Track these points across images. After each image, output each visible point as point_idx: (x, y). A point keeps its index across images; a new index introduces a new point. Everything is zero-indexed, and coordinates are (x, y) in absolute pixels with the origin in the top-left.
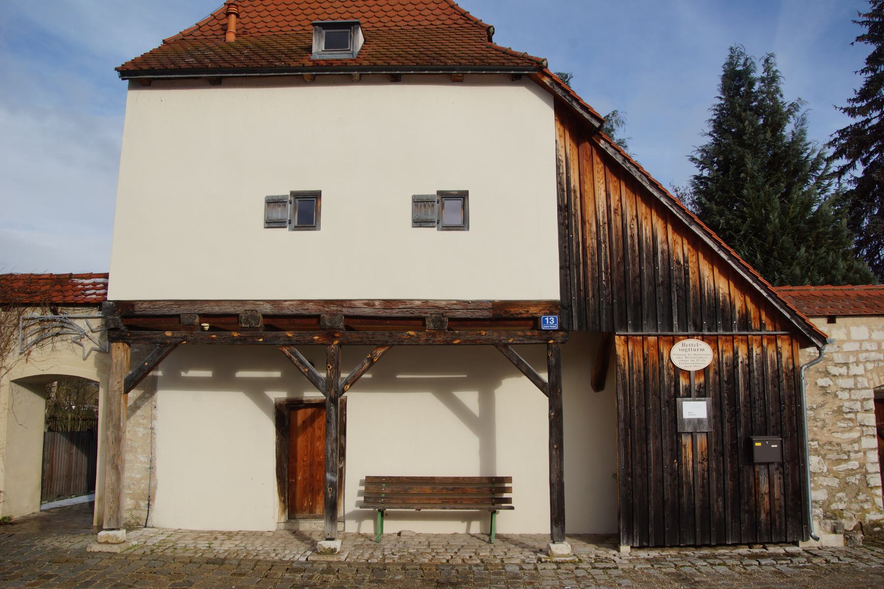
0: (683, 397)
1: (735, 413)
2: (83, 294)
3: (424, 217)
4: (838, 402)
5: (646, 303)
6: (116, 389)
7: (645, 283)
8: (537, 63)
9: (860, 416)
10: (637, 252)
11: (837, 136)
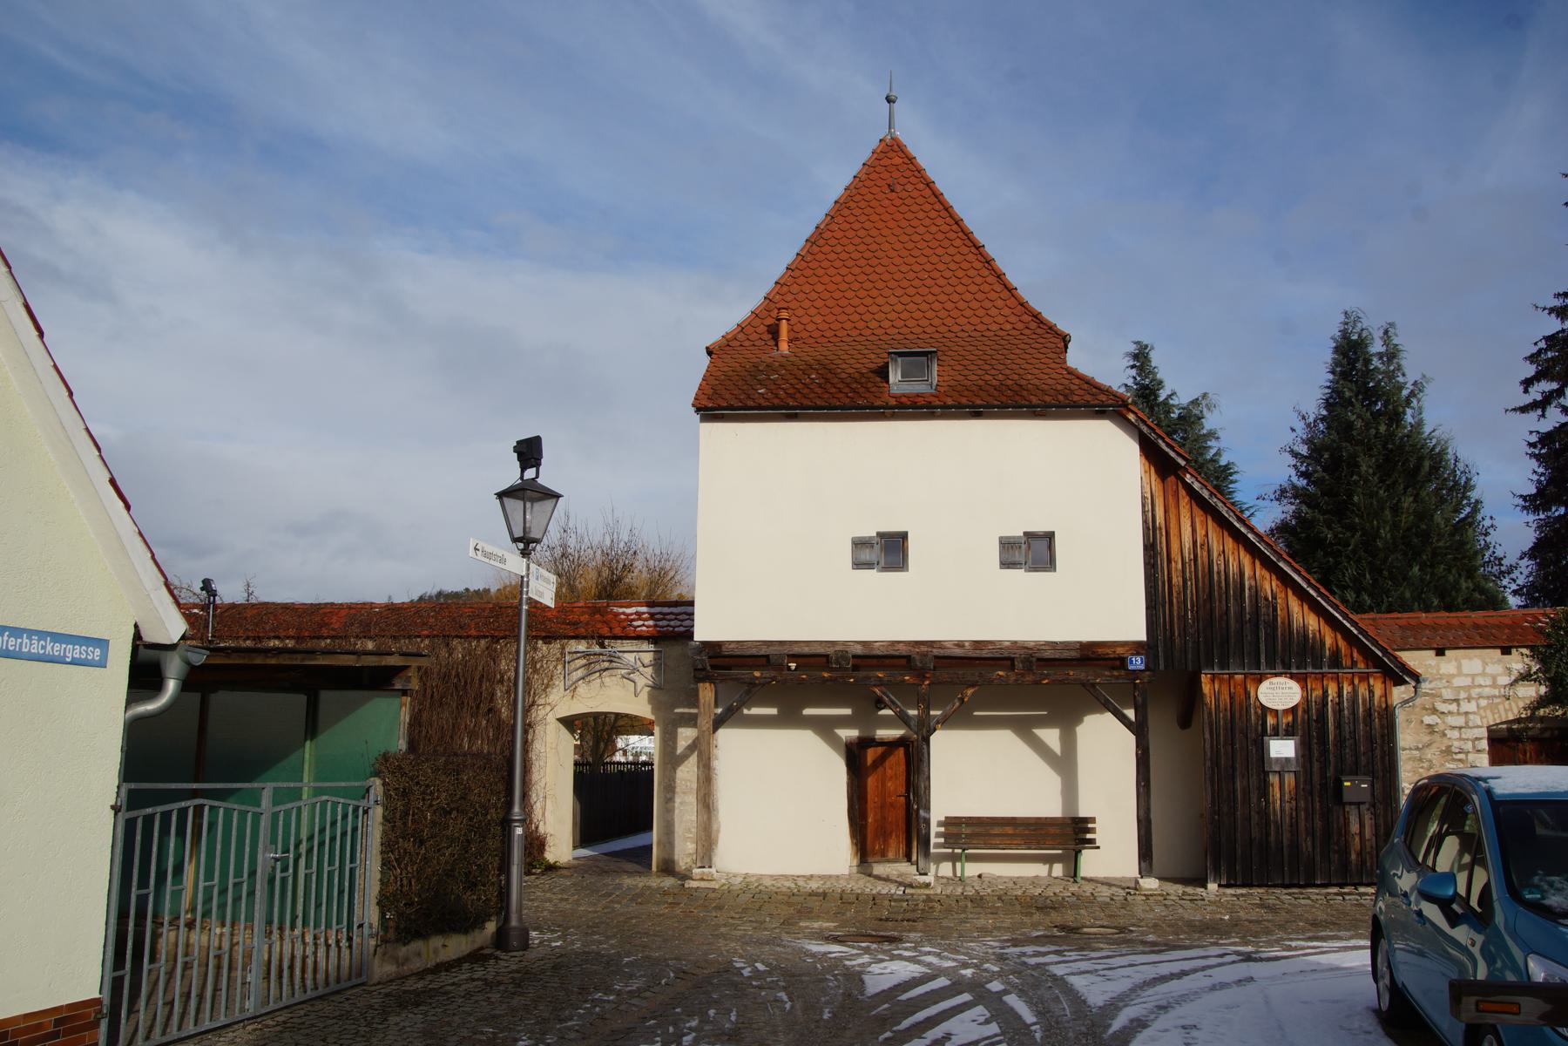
1: (1324, 752)
4: (1446, 742)
5: (1232, 641)
7: (1232, 621)
9: (1471, 757)
11: (1543, 345)
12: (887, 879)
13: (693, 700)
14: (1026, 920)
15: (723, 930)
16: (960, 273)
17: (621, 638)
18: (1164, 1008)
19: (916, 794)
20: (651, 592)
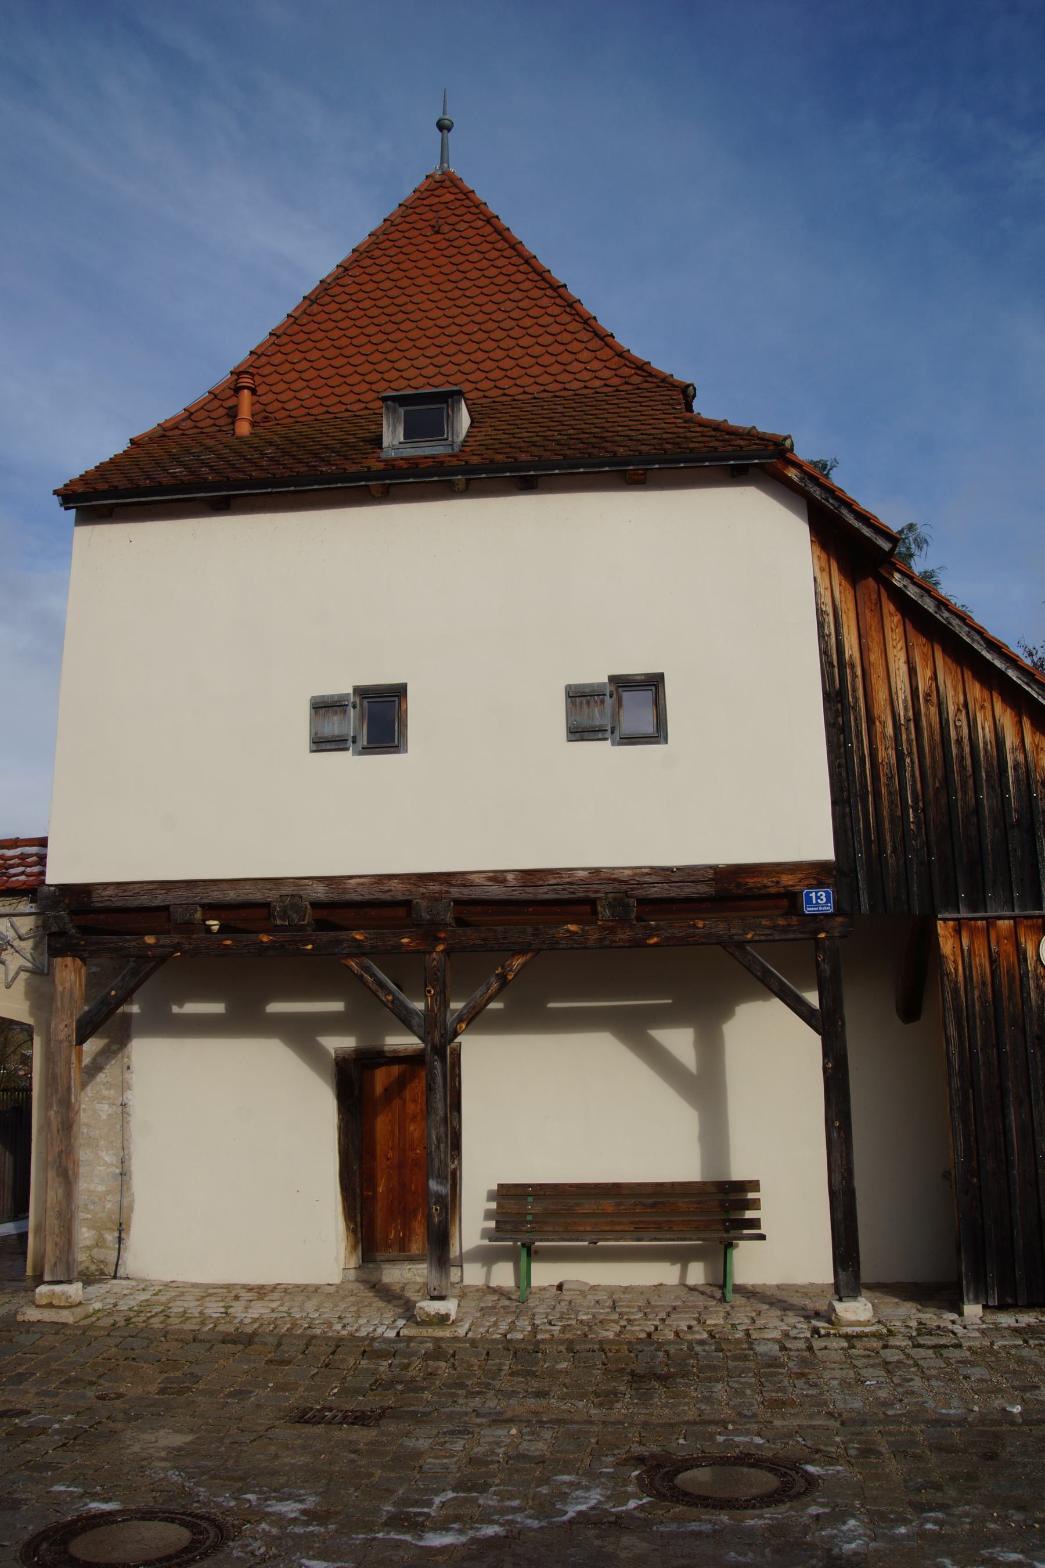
3: (586, 723)
7: (987, 824)
10: (969, 769)
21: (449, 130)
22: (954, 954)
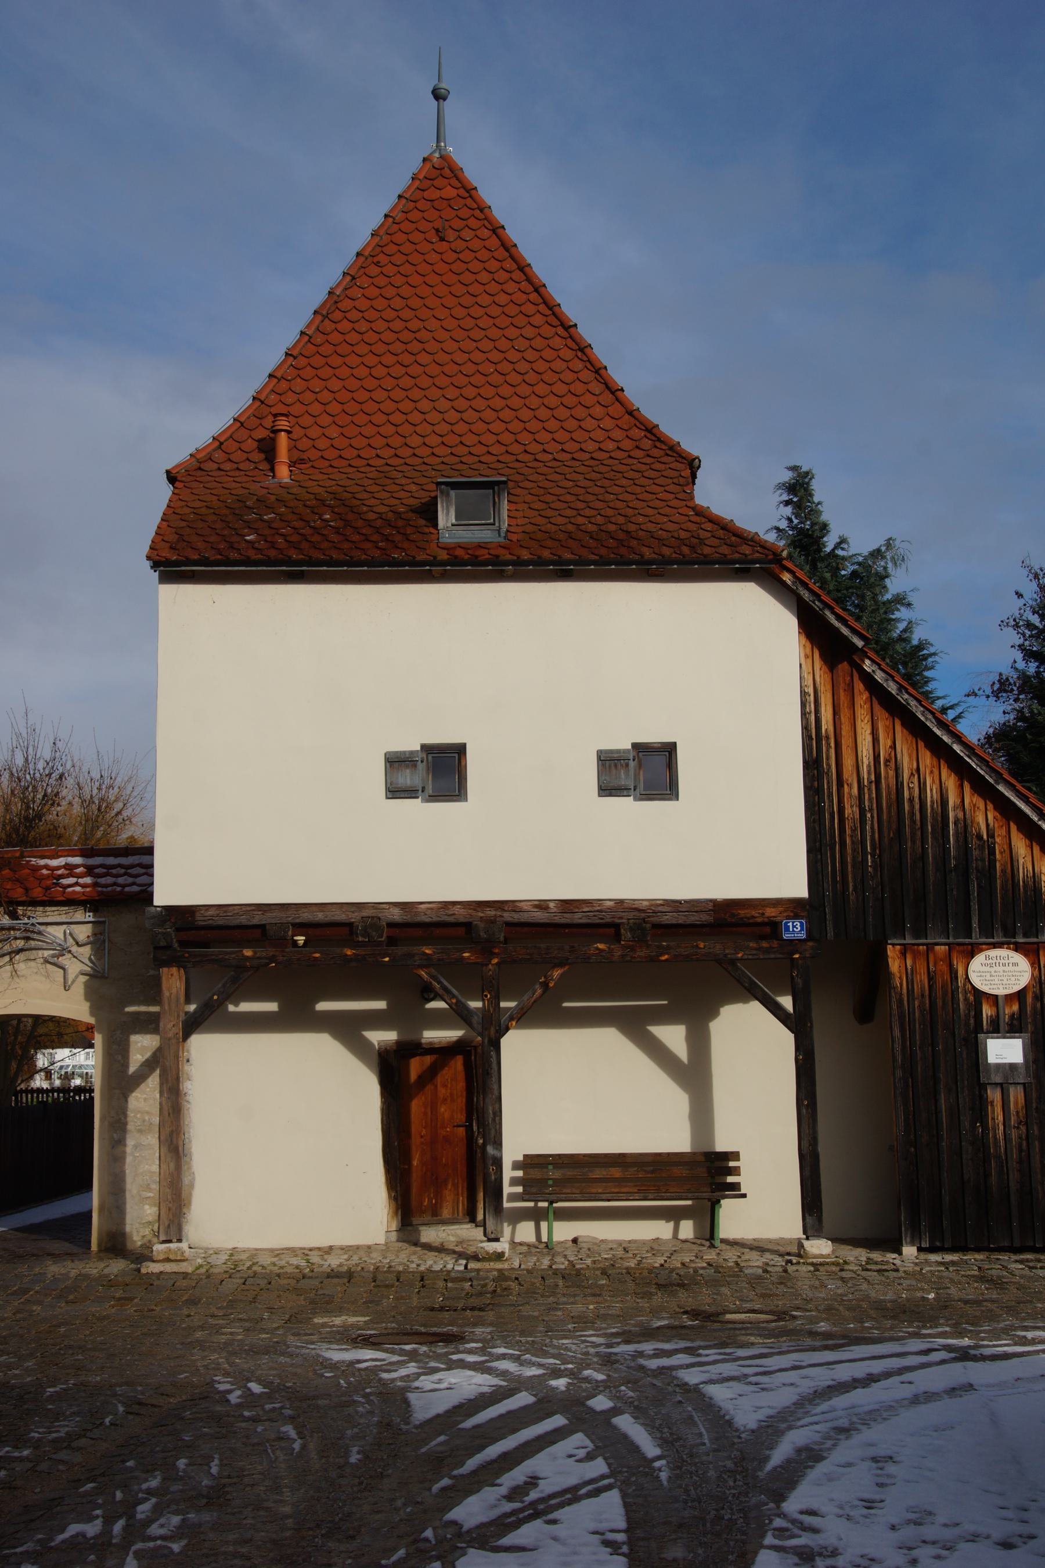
0: (988, 1032)
2: (57, 885)
3: (615, 783)
6: (170, 1034)
7: (931, 867)
8: (774, 554)
10: (919, 823)
12: (440, 1249)
13: (153, 992)
14: (644, 1303)
15: (199, 1334)
16: (541, 366)
17: (44, 904)
18: (845, 1431)
19: (482, 1124)
20: (86, 836)
21: (445, 100)
22: (900, 972)
